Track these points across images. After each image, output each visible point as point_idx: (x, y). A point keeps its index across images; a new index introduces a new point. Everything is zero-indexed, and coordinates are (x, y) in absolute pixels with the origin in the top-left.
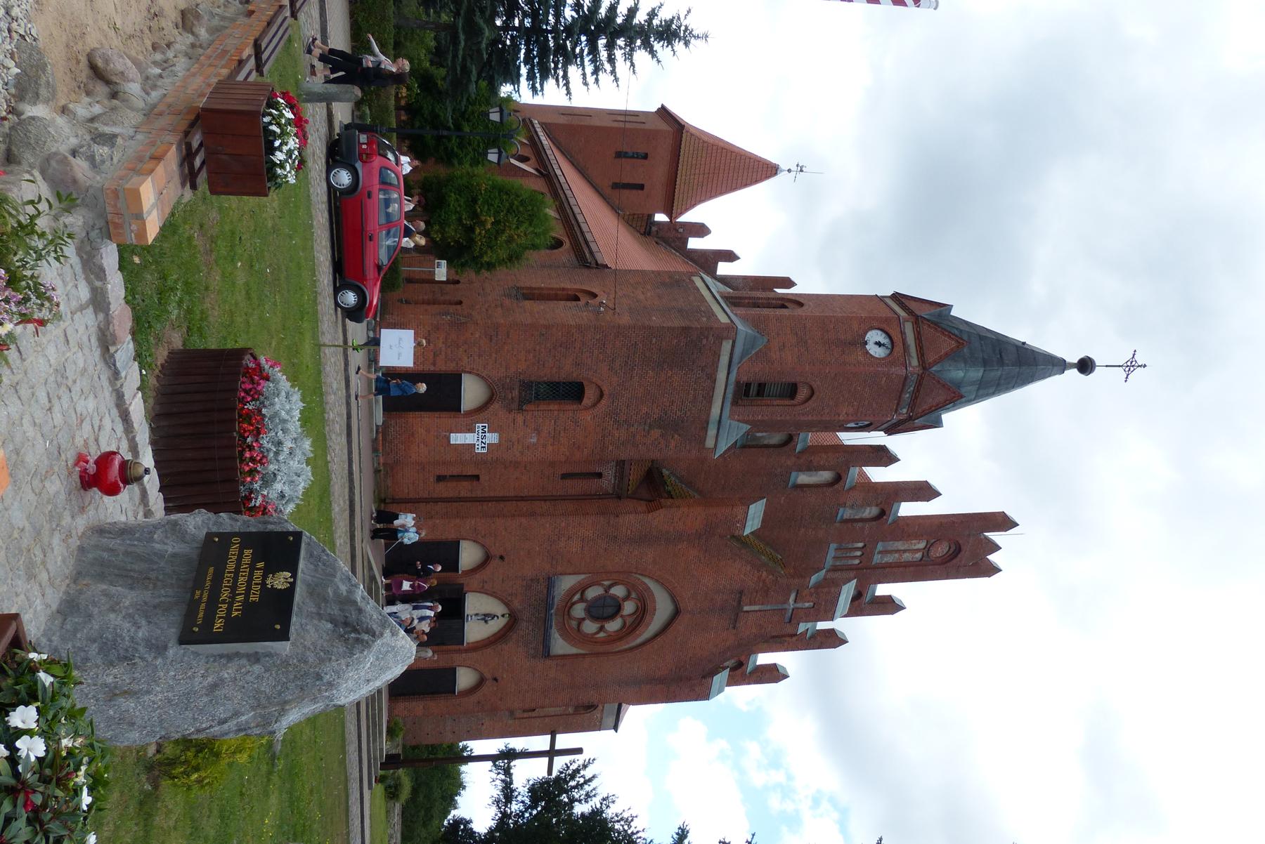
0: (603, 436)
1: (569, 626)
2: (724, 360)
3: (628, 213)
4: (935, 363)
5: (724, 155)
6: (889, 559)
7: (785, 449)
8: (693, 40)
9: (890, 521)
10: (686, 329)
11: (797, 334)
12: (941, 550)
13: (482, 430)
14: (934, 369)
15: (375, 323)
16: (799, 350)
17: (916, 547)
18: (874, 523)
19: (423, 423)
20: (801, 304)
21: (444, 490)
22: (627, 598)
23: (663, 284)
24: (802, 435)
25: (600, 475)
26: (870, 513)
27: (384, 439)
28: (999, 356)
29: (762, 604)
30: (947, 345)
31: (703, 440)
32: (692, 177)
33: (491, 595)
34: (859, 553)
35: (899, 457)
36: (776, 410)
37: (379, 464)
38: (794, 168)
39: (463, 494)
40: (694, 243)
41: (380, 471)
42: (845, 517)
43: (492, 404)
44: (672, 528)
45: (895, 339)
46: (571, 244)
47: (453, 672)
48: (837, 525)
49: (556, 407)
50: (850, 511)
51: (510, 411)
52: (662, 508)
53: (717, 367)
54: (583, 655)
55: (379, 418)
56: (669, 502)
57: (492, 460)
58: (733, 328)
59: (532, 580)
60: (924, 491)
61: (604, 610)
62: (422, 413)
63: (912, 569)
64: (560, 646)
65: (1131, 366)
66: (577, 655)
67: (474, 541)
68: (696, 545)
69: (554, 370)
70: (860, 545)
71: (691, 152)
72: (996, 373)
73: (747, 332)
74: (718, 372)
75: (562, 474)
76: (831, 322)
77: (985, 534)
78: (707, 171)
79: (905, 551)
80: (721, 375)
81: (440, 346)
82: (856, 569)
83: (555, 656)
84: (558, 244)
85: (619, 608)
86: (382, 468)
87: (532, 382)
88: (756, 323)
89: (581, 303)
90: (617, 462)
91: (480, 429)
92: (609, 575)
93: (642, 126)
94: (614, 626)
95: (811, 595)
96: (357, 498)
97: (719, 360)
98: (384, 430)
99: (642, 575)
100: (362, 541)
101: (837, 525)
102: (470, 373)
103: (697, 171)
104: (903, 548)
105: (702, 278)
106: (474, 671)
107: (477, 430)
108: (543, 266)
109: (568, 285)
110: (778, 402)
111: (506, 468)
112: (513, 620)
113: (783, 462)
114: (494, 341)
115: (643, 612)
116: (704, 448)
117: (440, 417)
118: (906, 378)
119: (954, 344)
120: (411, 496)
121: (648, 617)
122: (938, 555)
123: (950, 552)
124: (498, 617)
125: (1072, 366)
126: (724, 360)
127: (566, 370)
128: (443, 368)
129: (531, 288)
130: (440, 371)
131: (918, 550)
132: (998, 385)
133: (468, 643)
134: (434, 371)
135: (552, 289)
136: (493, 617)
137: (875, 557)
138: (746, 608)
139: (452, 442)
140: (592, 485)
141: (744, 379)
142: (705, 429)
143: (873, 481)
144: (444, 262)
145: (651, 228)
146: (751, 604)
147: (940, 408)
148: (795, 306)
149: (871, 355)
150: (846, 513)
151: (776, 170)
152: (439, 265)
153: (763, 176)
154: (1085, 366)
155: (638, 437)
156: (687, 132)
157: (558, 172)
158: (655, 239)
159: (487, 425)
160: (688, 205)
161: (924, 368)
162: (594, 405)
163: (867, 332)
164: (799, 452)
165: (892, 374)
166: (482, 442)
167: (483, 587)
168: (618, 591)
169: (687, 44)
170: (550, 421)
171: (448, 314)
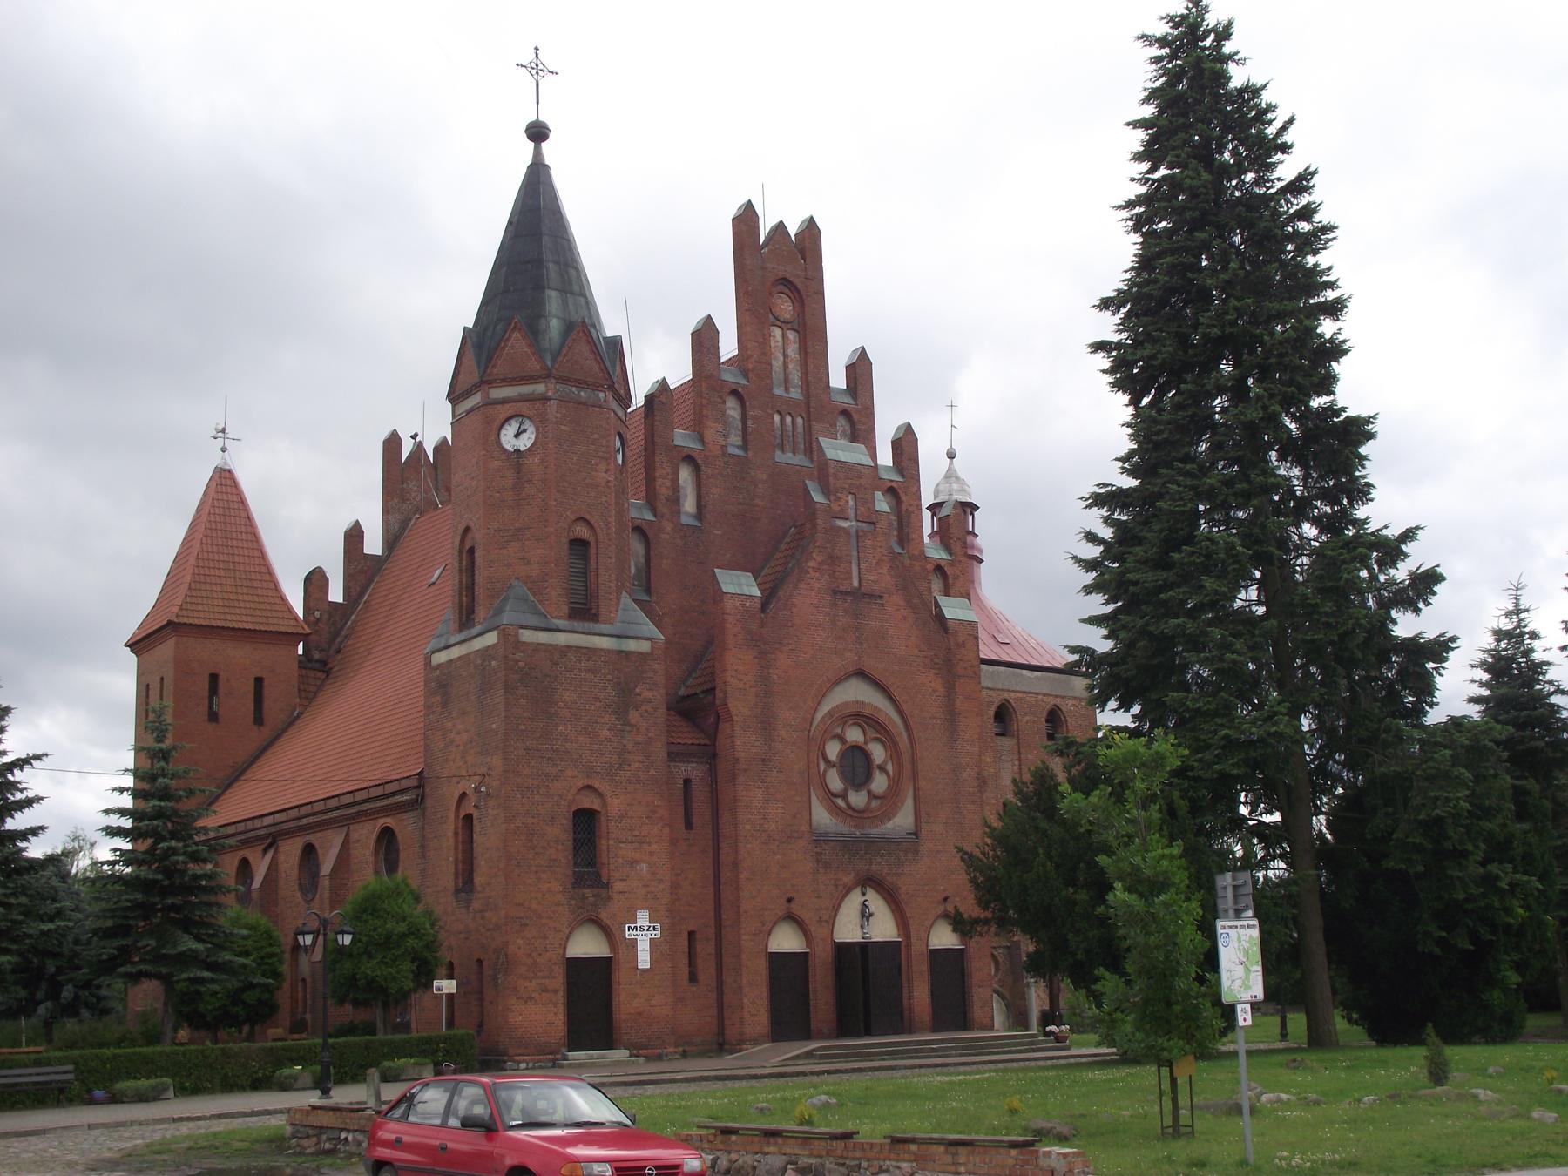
0: (639, 781)
2: (543, 637)
3: (298, 700)
6: (795, 376)
7: (650, 535)
9: (743, 382)
10: (508, 688)
12: (785, 307)
17: (779, 338)
18: (748, 404)
19: (627, 1002)
22: (842, 739)
25: (687, 782)
26: (734, 409)
28: (529, 266)
30: (517, 343)
31: (642, 656)
33: (837, 910)
34: (788, 419)
36: (605, 565)
38: (220, 442)
39: (711, 949)
40: (336, 594)
41: (684, 1051)
44: (752, 690)
47: (935, 954)
48: (750, 454)
51: (609, 898)
52: (726, 704)
53: (551, 645)
54: (916, 790)
55: (621, 1054)
56: (719, 694)
57: (668, 917)
58: (504, 630)
59: (818, 861)
60: (704, 337)
61: (857, 766)
64: (903, 820)
65: (537, 69)
66: (916, 799)
67: (769, 934)
68: (773, 656)
69: (560, 847)
70: (777, 418)
72: (552, 271)
75: (686, 828)
77: (762, 241)
78: (232, 581)
79: (785, 356)
80: (562, 639)
83: (916, 826)
85: (856, 748)
86: (681, 1049)
87: (575, 872)
89: (476, 814)
90: (671, 761)
92: (811, 765)
93: (168, 682)
94: (878, 753)
95: (839, 499)
98: (635, 1048)
99: (811, 724)
102: (565, 948)
104: (782, 358)
105: (434, 652)
108: (423, 856)
110: (593, 563)
112: (869, 881)
113: (668, 537)
114: (527, 922)
116: (652, 653)
120: (715, 1013)
121: (868, 711)
123: (787, 291)
124: (865, 901)
126: (543, 637)
127: (560, 832)
131: (784, 336)
132: (566, 265)
133: (899, 936)
135: (456, 849)
136: (864, 906)
138: (856, 584)
140: (698, 789)
141: (565, 609)
143: (691, 377)
144: (436, 983)
145: (317, 661)
146: (851, 578)
147: (597, 348)
148: (470, 535)
149: (533, 445)
151: (225, 470)
152: (439, 989)
154: (538, 133)
155: (640, 738)
157: (268, 821)
161: (548, 376)
162: (600, 795)
163: (503, 448)
164: (655, 516)
167: (826, 921)
168: (833, 750)
170: (621, 848)
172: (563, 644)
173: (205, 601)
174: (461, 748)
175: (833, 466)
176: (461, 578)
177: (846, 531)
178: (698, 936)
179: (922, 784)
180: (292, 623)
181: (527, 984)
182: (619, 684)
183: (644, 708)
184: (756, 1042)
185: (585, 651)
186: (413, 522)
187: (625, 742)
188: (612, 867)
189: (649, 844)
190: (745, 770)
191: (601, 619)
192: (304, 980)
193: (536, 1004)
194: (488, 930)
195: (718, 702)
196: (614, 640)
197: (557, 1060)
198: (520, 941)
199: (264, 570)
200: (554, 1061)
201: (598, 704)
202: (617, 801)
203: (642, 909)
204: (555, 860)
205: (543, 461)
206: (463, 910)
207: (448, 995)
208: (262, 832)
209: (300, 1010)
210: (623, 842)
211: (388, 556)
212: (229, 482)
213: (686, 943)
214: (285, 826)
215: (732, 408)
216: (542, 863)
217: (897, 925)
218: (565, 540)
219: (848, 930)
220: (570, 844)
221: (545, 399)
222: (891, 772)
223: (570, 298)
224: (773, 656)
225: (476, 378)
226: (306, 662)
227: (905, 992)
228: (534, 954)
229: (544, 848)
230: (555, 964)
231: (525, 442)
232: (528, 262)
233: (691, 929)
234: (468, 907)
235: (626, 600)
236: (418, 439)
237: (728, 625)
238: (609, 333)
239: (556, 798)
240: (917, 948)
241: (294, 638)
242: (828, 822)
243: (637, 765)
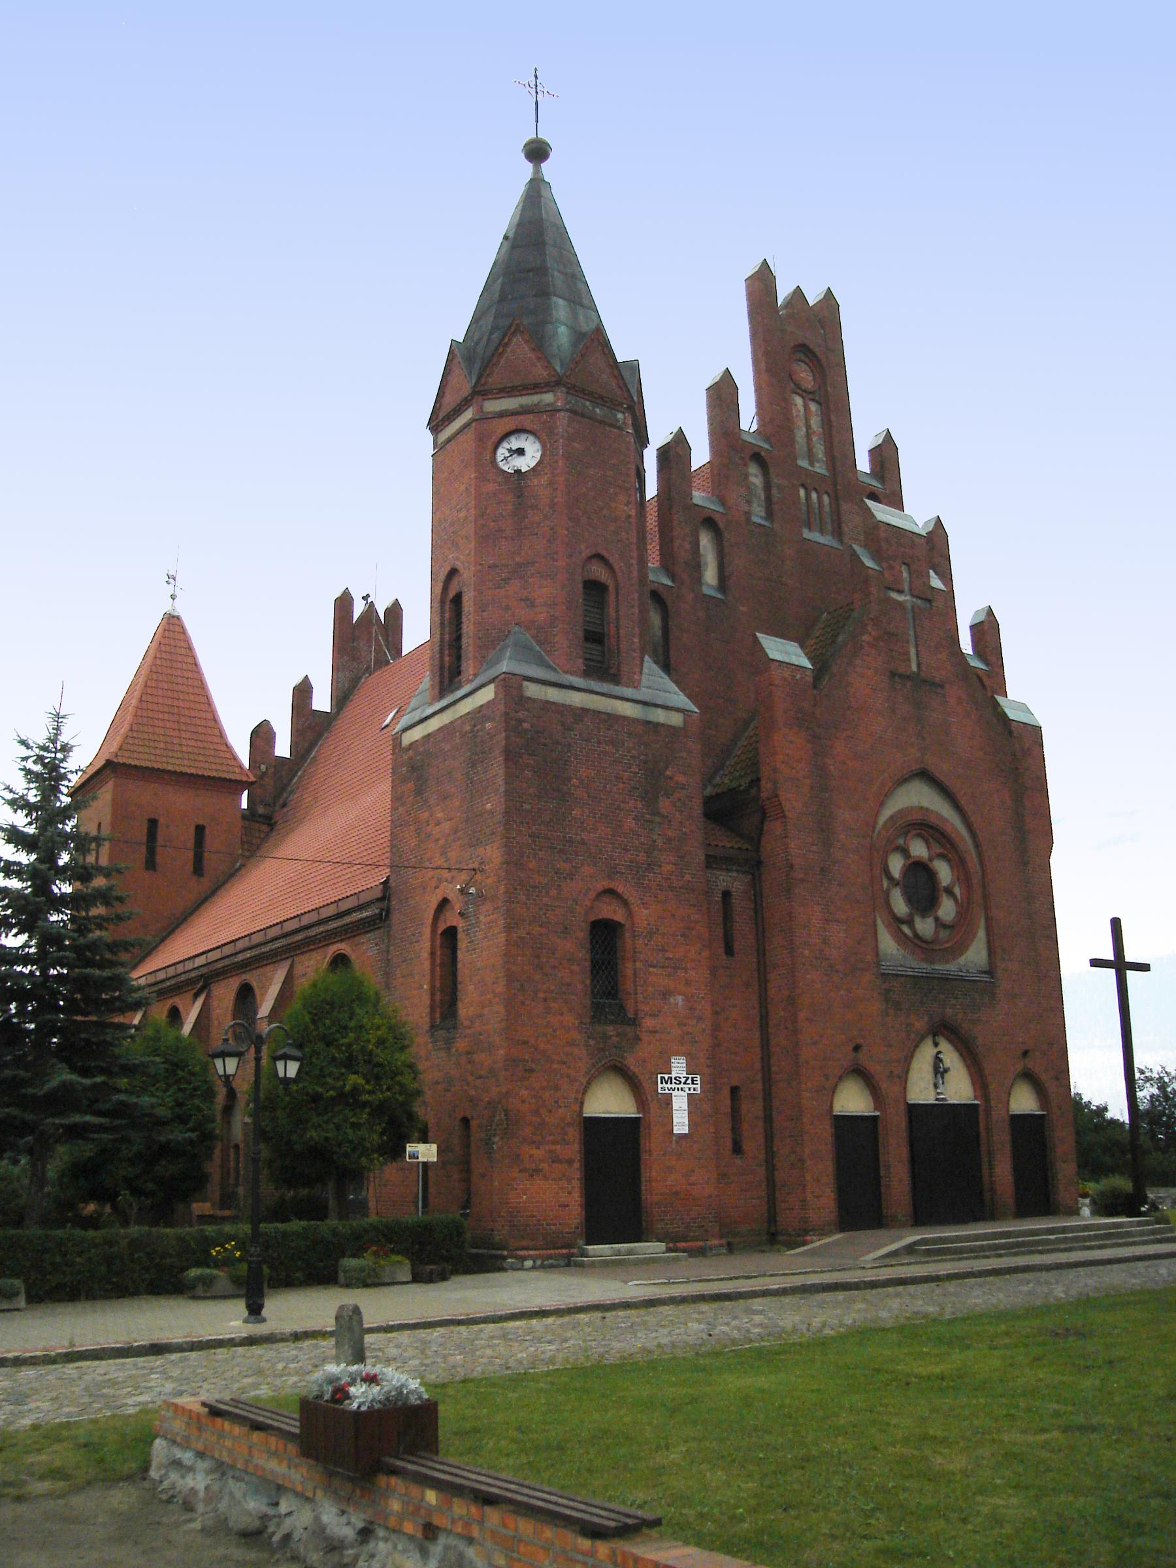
1: (947, 942)
2: (553, 695)
4: (548, 366)
5: (150, 698)
6: (819, 450)
7: (669, 603)
8: (64, 738)
9: (767, 446)
10: (510, 756)
11: (505, 580)
12: (805, 376)
13: (666, 1083)
14: (558, 368)
15: (511, 1257)
16: (532, 575)
17: (801, 409)
18: (771, 470)
20: (453, 572)
21: (753, 1144)
22: (905, 852)
23: (419, 792)
24: (651, 577)
25: (726, 895)
26: (756, 476)
27: (684, 1239)
29: (908, 642)
30: (520, 348)
32: (184, 749)
33: (910, 1063)
34: (814, 496)
35: (675, 430)
37: (721, 1245)
40: (283, 748)
42: (763, 514)
43: (629, 1069)
45: (512, 427)
46: (342, 940)
49: (629, 965)
50: (755, 505)
51: (638, 1039)
52: (777, 796)
53: (563, 705)
54: (988, 920)
56: (766, 785)
58: (504, 680)
59: (887, 1000)
62: (643, 1179)
63: (833, 418)
64: (975, 955)
66: (988, 934)
67: (834, 1092)
69: (575, 968)
71: (147, 750)
72: (558, 280)
73: (510, 658)
74: (571, 703)
76: (484, 525)
78: (176, 726)
79: (808, 427)
80: (576, 699)
81: (543, 1152)
82: (837, 500)
84: (340, 961)
88: (491, 643)
89: (461, 924)
90: (707, 867)
91: (666, 1086)
94: (944, 873)
95: (891, 568)
96: (798, 1281)
97: (553, 703)
98: (673, 1240)
99: (874, 828)
100: (863, 1268)
101: (776, 526)
102: (582, 1103)
103: (176, 741)
104: (804, 429)
105: (405, 730)
106: (838, 1091)
107: (667, 1091)
109: (426, 944)
111: (718, 1045)
112: (944, 1029)
114: (534, 1066)
115: (925, 827)
117: (650, 1151)
118: (573, 412)
119: (517, 339)
121: (932, 819)
122: (811, 378)
123: (807, 360)
124: (939, 1052)
125: (537, 170)
126: (553, 695)
128: (576, 1147)
129: (432, 1008)
130: (580, 1152)
132: (573, 276)
134: (580, 1161)
135: (433, 971)
136: (938, 1060)
137: (819, 471)
138: (914, 668)
139: (685, 1130)
140: (741, 905)
142: (655, 727)
144: (410, 1148)
145: (260, 816)
149: (538, 464)
150: (758, 514)
151: (173, 617)
153: (182, 637)
154: (537, 152)
156: (117, 756)
158: (277, 808)
159: (659, 1076)
160: (228, 755)
161: (558, 383)
162: (625, 903)
165: (567, 432)
166: (685, 1083)
168: (896, 865)
169: (66, 749)
171: (490, 1139)
172: (579, 706)
173: (147, 743)
174: (441, 842)
175: (883, 529)
176: (442, 634)
180: (237, 770)
181: (534, 1151)
182: (645, 762)
183: (676, 795)
184: (823, 1232)
185: (603, 716)
186: (363, 680)
187: (655, 837)
188: (640, 997)
189: (686, 970)
190: (802, 881)
191: (624, 679)
192: (237, 1147)
193: (546, 1178)
194: (480, 1077)
195: (764, 795)
196: (638, 707)
197: (573, 1255)
198: (524, 1093)
199: (209, 716)
200: (569, 1256)
201: (621, 785)
202: (645, 912)
204: (569, 985)
205: (551, 483)
206: (443, 1054)
207: (425, 1164)
208: (193, 974)
209: (232, 1181)
210: (654, 967)
211: (338, 713)
212: (177, 629)
213: (728, 1102)
214: (219, 965)
215: (756, 478)
217: (974, 1083)
218: (579, 579)
219: (921, 1091)
220: (588, 964)
221: (553, 411)
223: (581, 311)
225: (467, 390)
226: (250, 815)
227: (985, 1166)
228: (543, 1111)
230: (568, 1124)
231: (525, 463)
232: (529, 271)
233: (735, 1083)
234: (449, 1049)
235: (649, 664)
236: (369, 601)
239: (570, 903)
240: (998, 1114)
241: (237, 786)
242: (895, 952)
243: (669, 867)
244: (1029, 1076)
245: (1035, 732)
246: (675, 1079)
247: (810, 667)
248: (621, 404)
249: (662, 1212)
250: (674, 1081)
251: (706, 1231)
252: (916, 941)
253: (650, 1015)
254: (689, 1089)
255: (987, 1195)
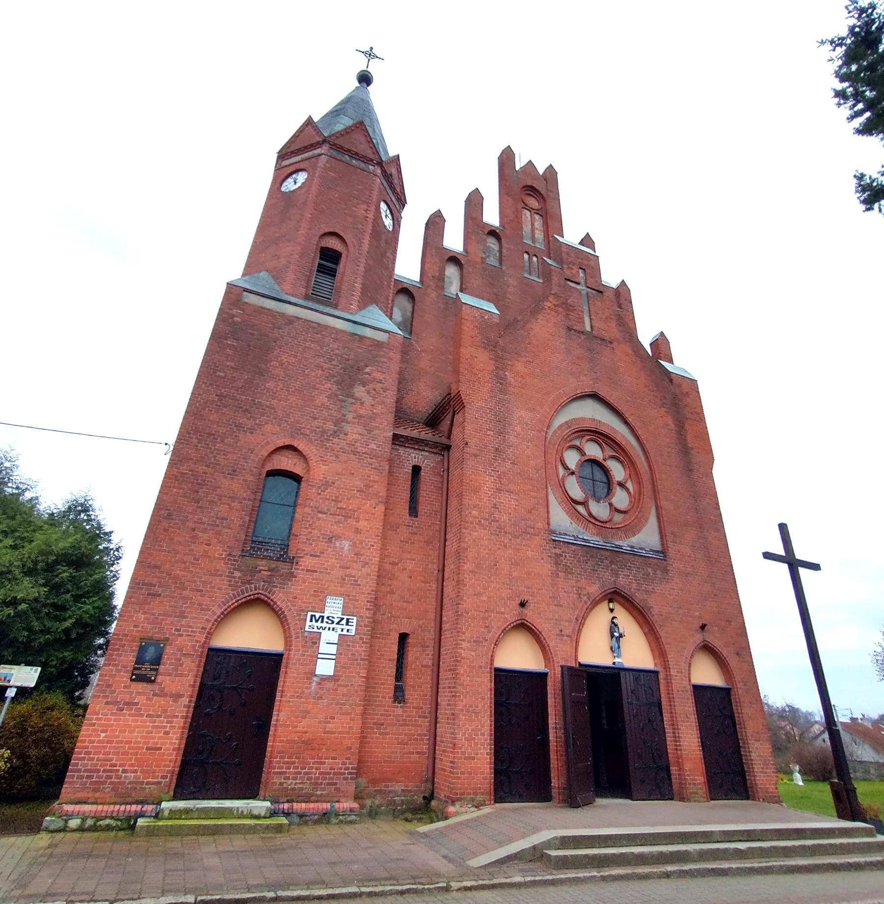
6: (539, 235)
13: (317, 621)
22: (580, 450)
25: (416, 470)
31: (378, 344)
39: (428, 660)
47: (699, 690)
51: (292, 575)
59: (557, 564)
65: (370, 54)
68: (510, 363)
69: (235, 504)
79: (533, 225)
80: (291, 310)
83: (662, 544)
94: (618, 471)
99: (548, 427)
107: (316, 630)
112: (615, 596)
124: (614, 618)
136: (614, 625)
138: (588, 328)
141: (303, 291)
166: (338, 623)
168: (572, 459)
170: (319, 519)
177: (579, 292)
178: (410, 640)
179: (663, 503)
183: (371, 386)
188: (303, 538)
190: (476, 456)
191: (339, 307)
203: (336, 595)
213: (395, 648)
216: (204, 519)
222: (631, 490)
224: (510, 363)
229: (212, 502)
237: (465, 328)
238: (392, 153)
244: (707, 649)
245: (694, 382)
246: (328, 618)
247: (498, 313)
248: (372, 160)
249: (285, 763)
250: (325, 620)
251: (338, 790)
252: (589, 519)
253: (311, 555)
254: (342, 630)
255: (674, 769)
